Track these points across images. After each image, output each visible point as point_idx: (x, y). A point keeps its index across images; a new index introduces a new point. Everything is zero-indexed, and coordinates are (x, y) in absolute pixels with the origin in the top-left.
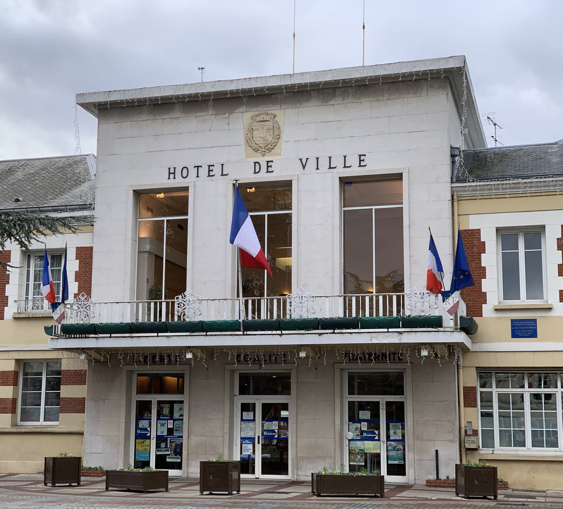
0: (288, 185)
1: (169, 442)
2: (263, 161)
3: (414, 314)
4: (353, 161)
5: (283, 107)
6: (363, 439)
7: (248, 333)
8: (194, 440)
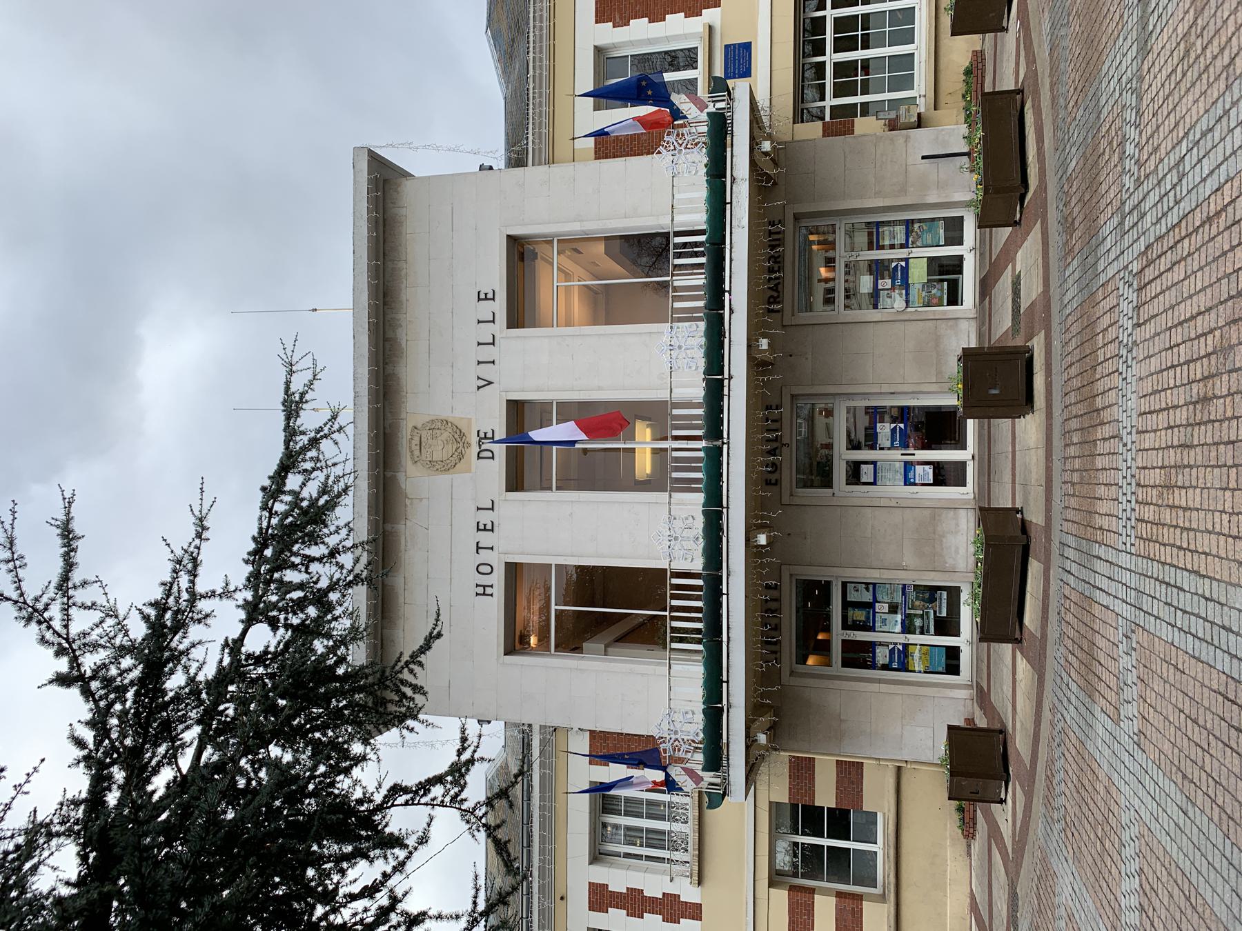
1: (912, 612)
4: (485, 309)
5: (403, 415)
6: (906, 285)
7: (725, 435)
8: (909, 560)
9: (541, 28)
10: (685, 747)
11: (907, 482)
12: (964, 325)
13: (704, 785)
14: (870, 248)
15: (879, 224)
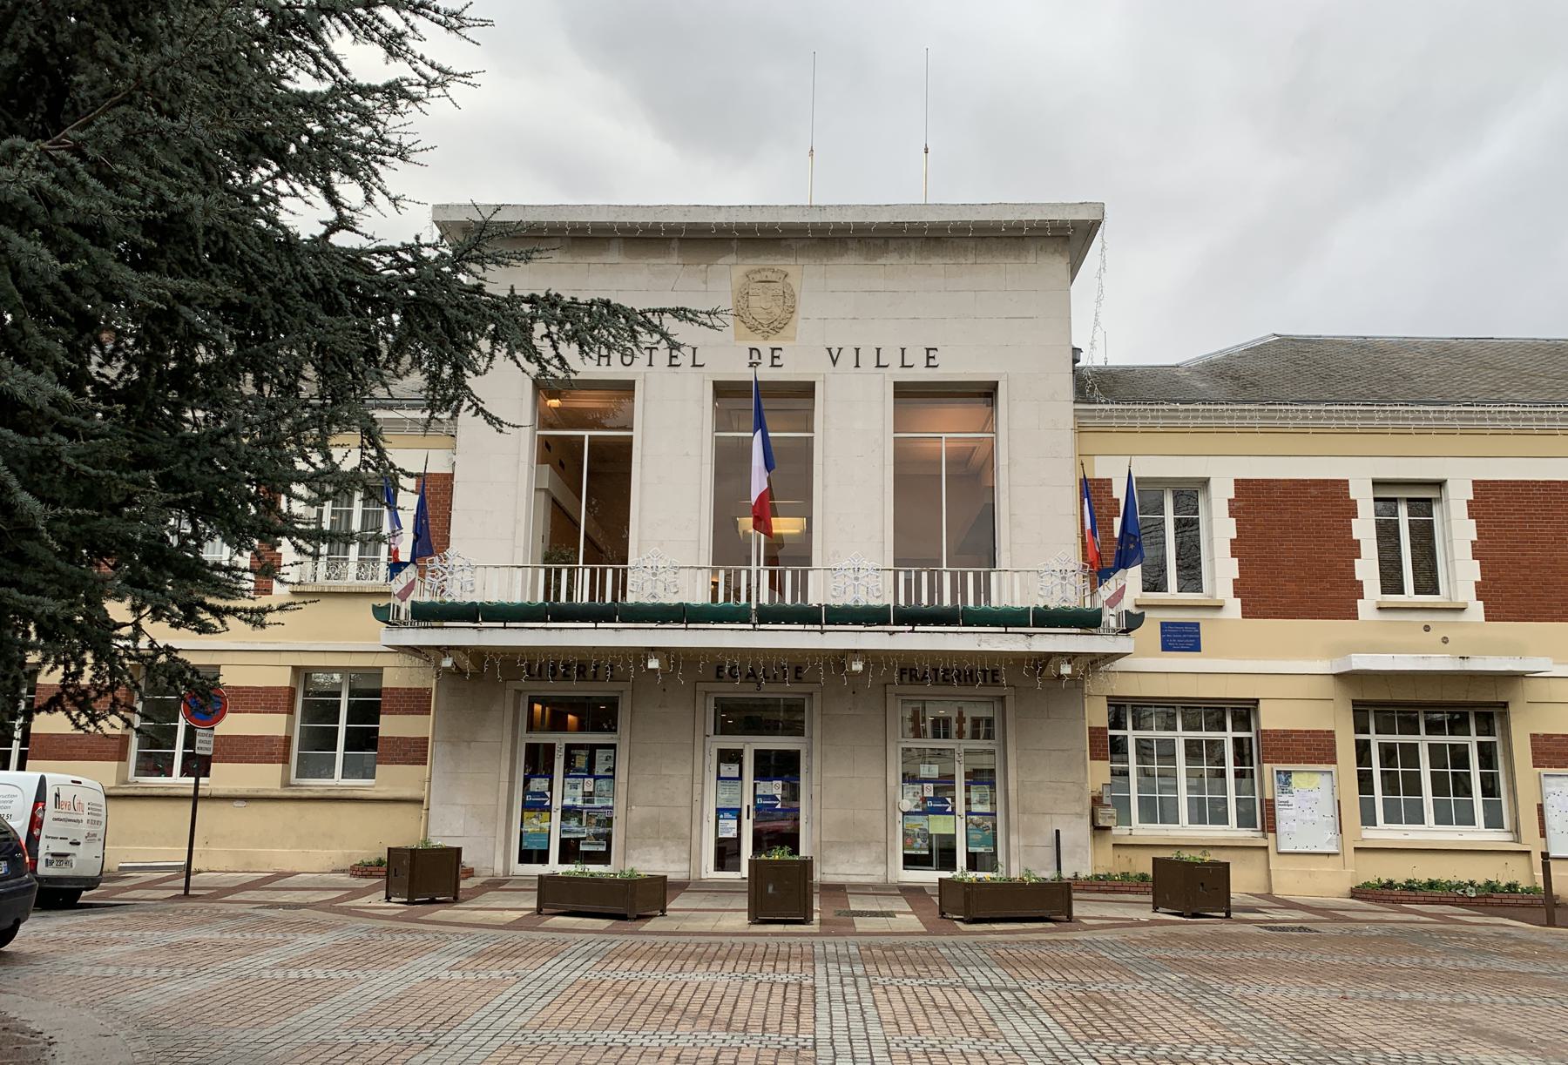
0: (805, 391)
2: (765, 347)
3: (646, 600)
4: (917, 357)
5: (800, 261)
6: (925, 812)
8: (637, 812)
9: (1231, 418)
10: (436, 582)
11: (719, 811)
12: (880, 870)
13: (397, 601)
15: (992, 785)
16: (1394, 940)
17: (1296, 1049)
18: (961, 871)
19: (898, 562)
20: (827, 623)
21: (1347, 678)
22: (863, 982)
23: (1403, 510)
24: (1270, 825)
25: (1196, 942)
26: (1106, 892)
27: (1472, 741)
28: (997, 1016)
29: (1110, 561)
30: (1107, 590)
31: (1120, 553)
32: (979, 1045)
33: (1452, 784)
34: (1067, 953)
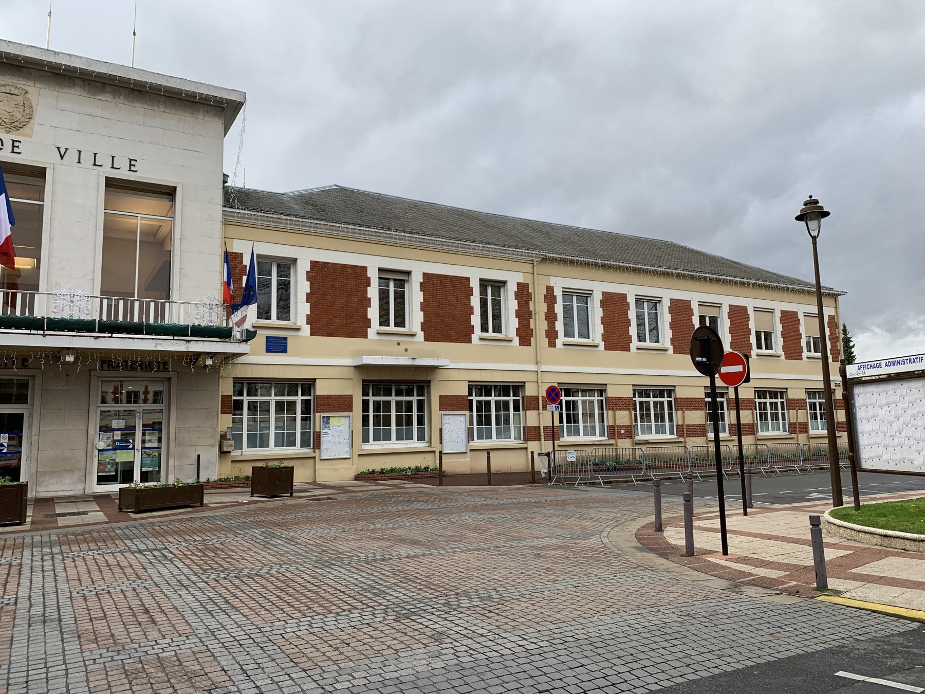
0: (40, 173)
5: (38, 85)
6: (114, 449)
14: (144, 426)
15: (160, 430)
16: (373, 499)
17: (316, 561)
18: (137, 482)
19: (102, 293)
20: (48, 330)
21: (360, 368)
22: (58, 558)
23: (392, 284)
24: (317, 446)
25: (272, 511)
26: (226, 488)
27: (414, 399)
28: (148, 566)
29: (239, 300)
30: (235, 318)
31: (244, 296)
32: (134, 585)
33: (405, 421)
34: (197, 524)
